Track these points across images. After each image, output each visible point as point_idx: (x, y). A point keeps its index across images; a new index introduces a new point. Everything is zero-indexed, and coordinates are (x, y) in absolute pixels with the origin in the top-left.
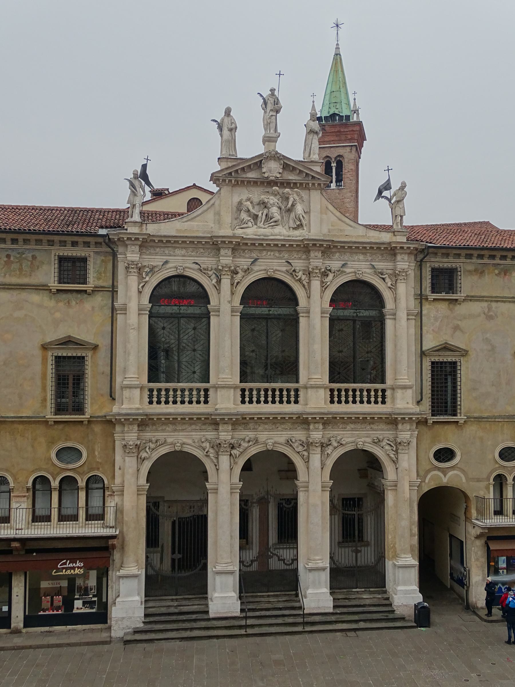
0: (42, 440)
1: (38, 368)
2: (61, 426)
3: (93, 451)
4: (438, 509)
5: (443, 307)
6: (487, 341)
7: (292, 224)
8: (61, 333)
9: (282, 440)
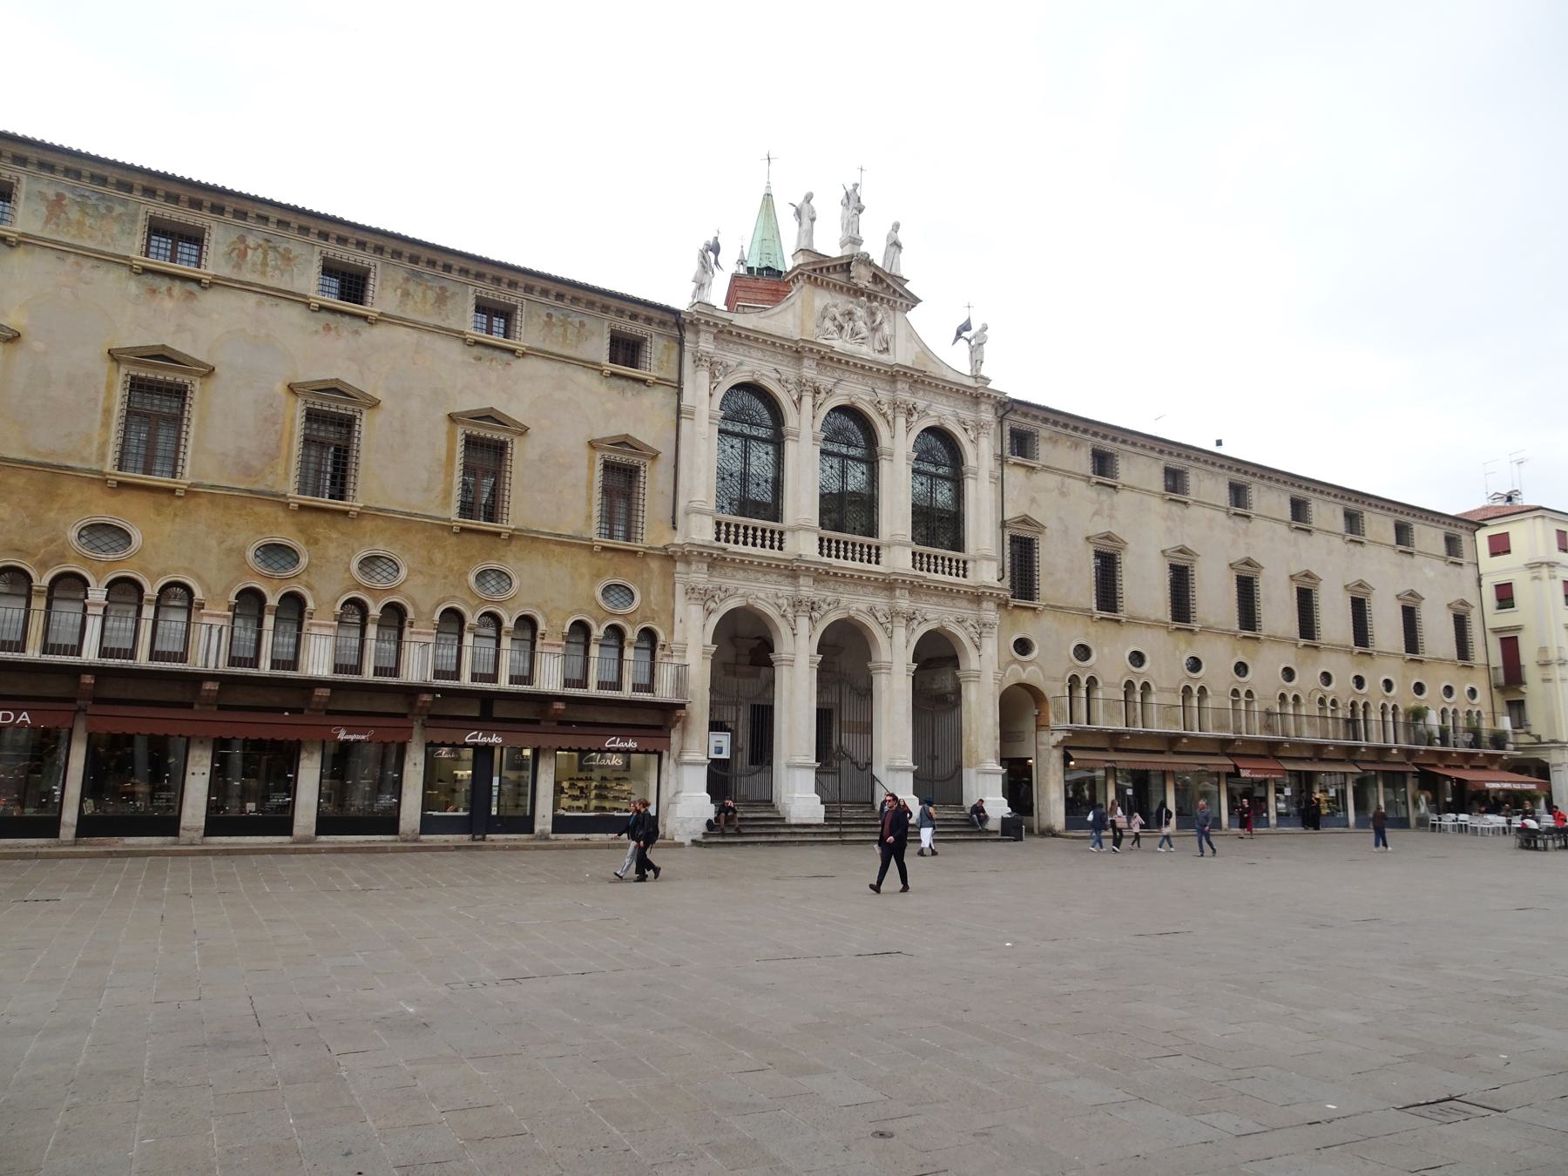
0: (584, 570)
1: (583, 471)
2: (609, 555)
3: (648, 594)
4: (1019, 705)
5: (1021, 472)
6: (1060, 519)
7: (878, 347)
8: (616, 429)
9: (863, 607)
